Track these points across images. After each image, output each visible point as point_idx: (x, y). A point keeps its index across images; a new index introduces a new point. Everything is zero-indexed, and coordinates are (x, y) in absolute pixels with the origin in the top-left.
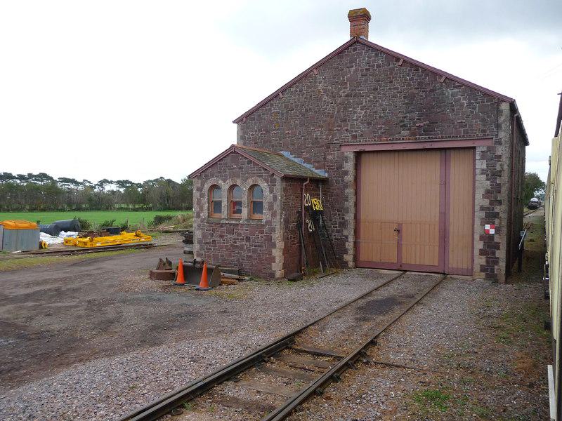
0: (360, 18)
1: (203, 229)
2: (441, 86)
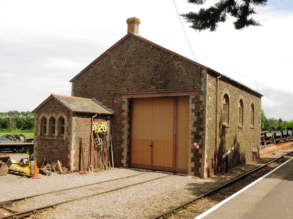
0: (132, 23)
1: (38, 142)
2: (172, 59)
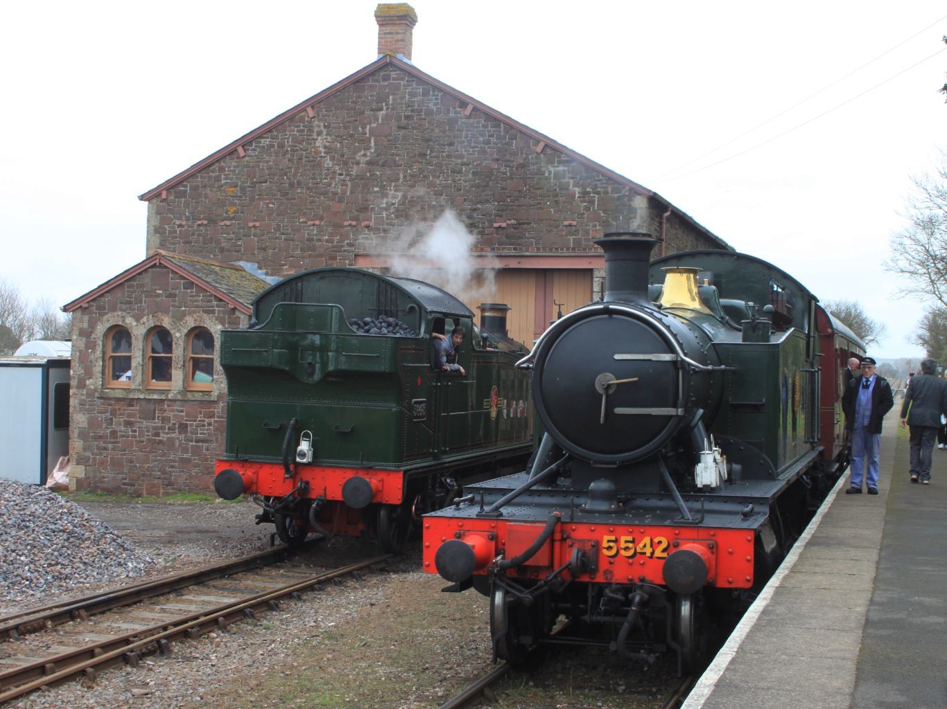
1: (89, 411)
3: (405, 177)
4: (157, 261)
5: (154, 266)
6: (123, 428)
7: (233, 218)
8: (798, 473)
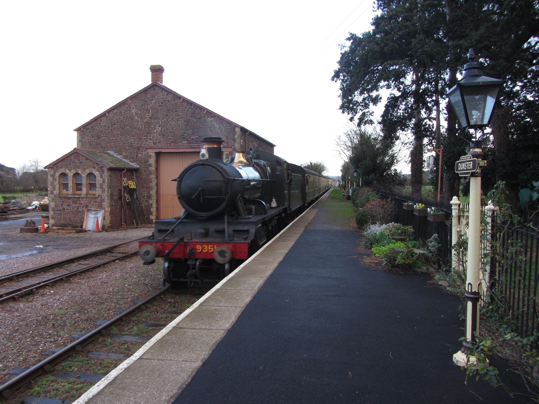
1: (55, 202)
3: (162, 122)
4: (76, 151)
5: (75, 153)
6: (67, 207)
7: (105, 137)
8: (271, 215)
